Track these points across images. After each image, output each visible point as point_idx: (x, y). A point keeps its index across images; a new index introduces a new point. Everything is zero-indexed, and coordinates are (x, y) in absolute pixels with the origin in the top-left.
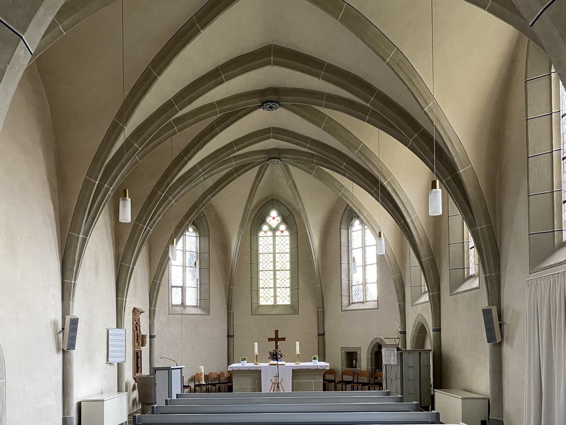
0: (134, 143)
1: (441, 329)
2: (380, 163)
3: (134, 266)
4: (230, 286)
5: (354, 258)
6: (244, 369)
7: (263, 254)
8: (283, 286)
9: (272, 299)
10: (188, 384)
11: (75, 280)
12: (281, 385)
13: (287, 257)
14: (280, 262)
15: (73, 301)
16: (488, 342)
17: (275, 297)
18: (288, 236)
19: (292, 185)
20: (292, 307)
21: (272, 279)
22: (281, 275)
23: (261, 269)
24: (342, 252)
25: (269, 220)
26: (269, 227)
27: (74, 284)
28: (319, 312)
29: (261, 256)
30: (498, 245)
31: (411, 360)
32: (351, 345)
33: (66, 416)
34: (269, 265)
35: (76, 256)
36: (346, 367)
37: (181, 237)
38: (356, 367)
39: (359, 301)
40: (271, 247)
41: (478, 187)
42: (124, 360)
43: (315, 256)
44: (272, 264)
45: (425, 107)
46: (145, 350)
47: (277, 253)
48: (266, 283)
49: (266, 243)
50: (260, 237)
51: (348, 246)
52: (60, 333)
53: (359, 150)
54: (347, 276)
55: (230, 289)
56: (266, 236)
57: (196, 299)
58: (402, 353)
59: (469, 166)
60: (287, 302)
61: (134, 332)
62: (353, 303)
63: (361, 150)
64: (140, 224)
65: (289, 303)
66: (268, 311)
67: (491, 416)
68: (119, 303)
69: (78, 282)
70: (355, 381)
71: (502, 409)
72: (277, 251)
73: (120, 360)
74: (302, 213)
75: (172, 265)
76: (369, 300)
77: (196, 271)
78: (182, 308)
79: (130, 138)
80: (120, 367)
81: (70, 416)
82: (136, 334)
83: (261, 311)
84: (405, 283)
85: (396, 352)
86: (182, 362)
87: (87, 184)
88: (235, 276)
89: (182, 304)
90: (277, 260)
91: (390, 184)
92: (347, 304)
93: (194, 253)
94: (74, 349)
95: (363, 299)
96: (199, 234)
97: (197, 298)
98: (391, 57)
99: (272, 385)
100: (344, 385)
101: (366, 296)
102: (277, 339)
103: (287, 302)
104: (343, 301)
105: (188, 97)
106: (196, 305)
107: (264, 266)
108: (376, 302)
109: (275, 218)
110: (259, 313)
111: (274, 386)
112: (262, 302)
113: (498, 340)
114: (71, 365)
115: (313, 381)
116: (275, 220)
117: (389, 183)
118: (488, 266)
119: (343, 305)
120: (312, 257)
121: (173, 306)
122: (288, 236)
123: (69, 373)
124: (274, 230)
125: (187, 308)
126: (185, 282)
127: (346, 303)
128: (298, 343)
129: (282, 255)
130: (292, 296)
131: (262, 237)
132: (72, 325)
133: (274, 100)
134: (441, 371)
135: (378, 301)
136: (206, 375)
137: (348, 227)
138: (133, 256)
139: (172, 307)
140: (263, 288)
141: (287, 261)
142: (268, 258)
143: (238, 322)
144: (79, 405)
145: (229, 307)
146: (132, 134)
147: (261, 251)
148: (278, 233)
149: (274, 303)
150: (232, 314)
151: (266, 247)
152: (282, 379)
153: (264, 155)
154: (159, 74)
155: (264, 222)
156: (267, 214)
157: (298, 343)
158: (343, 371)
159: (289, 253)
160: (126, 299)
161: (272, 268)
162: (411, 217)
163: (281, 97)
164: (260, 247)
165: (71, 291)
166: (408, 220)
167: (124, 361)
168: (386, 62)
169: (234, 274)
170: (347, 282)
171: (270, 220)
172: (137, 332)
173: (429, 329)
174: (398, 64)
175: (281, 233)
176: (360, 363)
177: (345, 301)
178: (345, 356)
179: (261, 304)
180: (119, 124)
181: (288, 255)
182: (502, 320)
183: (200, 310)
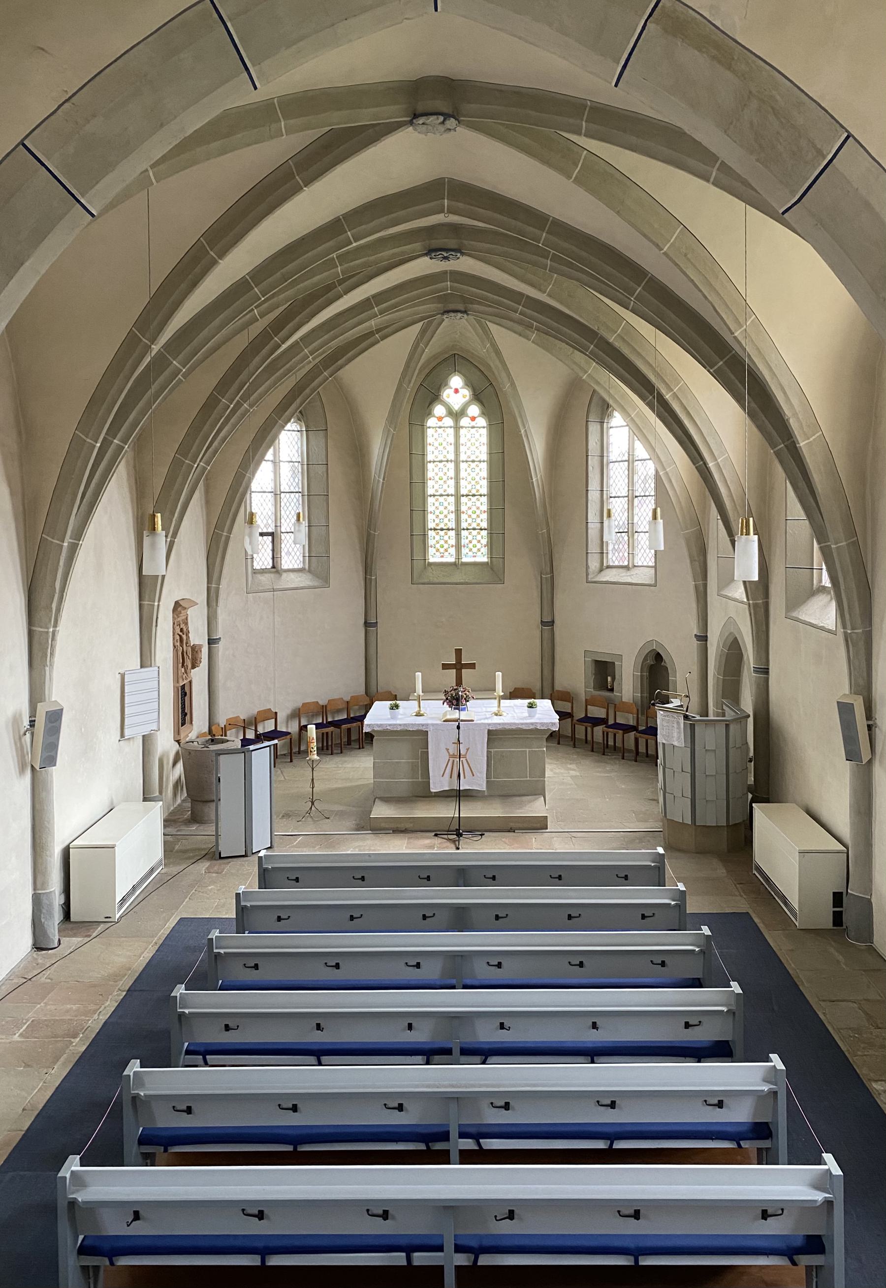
0: (172, 360)
1: (768, 669)
2: (659, 358)
3: (175, 538)
4: (369, 526)
5: (609, 511)
6: (395, 729)
7: (434, 462)
8: (474, 525)
9: (453, 551)
10: (287, 727)
11: (55, 626)
12: (466, 760)
13: (483, 470)
14: (469, 479)
15: (51, 665)
16: (847, 760)
17: (458, 547)
18: (484, 427)
19: (491, 350)
20: (492, 569)
21: (452, 512)
22: (469, 504)
23: (430, 491)
24: (590, 468)
25: (447, 394)
26: (446, 409)
27: (54, 633)
28: (544, 581)
29: (430, 466)
30: (869, 577)
31: (710, 738)
32: (605, 648)
33: (40, 892)
34: (446, 485)
35: (57, 581)
36: (594, 688)
37: (270, 447)
38: (612, 690)
39: (621, 564)
40: (451, 449)
41: (833, 472)
42: (155, 728)
43: (537, 477)
44: (452, 483)
45: (736, 331)
46: (199, 677)
47: (463, 462)
48: (441, 520)
49: (440, 440)
50: (429, 428)
51: (602, 456)
52: (25, 734)
53: (618, 335)
54: (598, 514)
55: (369, 535)
56: (440, 427)
57: (302, 555)
58: (694, 724)
59: (818, 434)
60: (482, 557)
61: (177, 651)
62: (608, 567)
63: (623, 335)
64: (186, 460)
65: (485, 559)
66: (444, 576)
67: (850, 890)
68: (146, 609)
69: (60, 628)
70: (611, 722)
71: (871, 880)
72: (463, 457)
73: (146, 730)
74: (511, 400)
75: (253, 492)
76: (640, 564)
77: (299, 531)
78: (272, 575)
79: (164, 350)
80: (147, 741)
81: (48, 891)
82: (180, 653)
83: (431, 575)
84: (708, 544)
85: (683, 721)
86: (274, 683)
87: (76, 447)
88: (379, 510)
89: (273, 567)
90: (463, 474)
91: (678, 397)
92: (597, 569)
93: (296, 464)
94: (55, 765)
95: (629, 562)
96: (307, 426)
97: (304, 553)
98: (672, 243)
99: (449, 760)
100: (589, 729)
101: (633, 557)
102: (459, 667)
103: (482, 557)
104: (590, 564)
105: (279, 273)
106: (301, 566)
107: (437, 487)
108: (653, 571)
109: (460, 390)
110: (426, 581)
111: (453, 761)
112: (434, 557)
113: (866, 757)
114: (49, 791)
115: (528, 750)
116: (459, 395)
117: (675, 396)
118: (850, 615)
119: (590, 570)
120: (530, 478)
121: (255, 572)
122: (484, 427)
123: (45, 808)
124: (457, 415)
125: (284, 575)
126: (279, 525)
127: (596, 567)
128: (499, 675)
129: (473, 465)
130: (491, 545)
131: (433, 428)
132: (51, 722)
133: (452, 247)
134: (768, 767)
135: (655, 567)
136: (323, 706)
137: (602, 419)
138: (172, 520)
139: (252, 577)
140: (435, 529)
141: (482, 443)
142: (445, 470)
143: (385, 597)
144: (66, 854)
145: (368, 568)
146: (168, 343)
147: (430, 457)
148: (465, 421)
149: (456, 559)
150: (373, 583)
151: (441, 448)
152: (469, 748)
153: (435, 305)
154: (222, 254)
155: (438, 398)
156: (442, 384)
157: (499, 675)
158: (588, 698)
159: (487, 495)
160: (159, 601)
161: (452, 491)
162: (716, 460)
163: (466, 242)
164: (429, 449)
165: (48, 648)
166: (711, 465)
167: (156, 729)
168: (662, 252)
169: (377, 508)
170: (599, 525)
171: (448, 397)
172: (181, 648)
173: (748, 655)
174: (686, 255)
175: (470, 421)
176: (620, 684)
177: (594, 564)
178: (591, 668)
179: (430, 561)
180: (141, 340)
181: (484, 466)
182: (873, 719)
183: (310, 577)
